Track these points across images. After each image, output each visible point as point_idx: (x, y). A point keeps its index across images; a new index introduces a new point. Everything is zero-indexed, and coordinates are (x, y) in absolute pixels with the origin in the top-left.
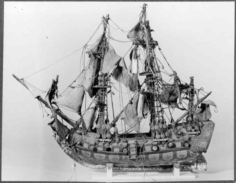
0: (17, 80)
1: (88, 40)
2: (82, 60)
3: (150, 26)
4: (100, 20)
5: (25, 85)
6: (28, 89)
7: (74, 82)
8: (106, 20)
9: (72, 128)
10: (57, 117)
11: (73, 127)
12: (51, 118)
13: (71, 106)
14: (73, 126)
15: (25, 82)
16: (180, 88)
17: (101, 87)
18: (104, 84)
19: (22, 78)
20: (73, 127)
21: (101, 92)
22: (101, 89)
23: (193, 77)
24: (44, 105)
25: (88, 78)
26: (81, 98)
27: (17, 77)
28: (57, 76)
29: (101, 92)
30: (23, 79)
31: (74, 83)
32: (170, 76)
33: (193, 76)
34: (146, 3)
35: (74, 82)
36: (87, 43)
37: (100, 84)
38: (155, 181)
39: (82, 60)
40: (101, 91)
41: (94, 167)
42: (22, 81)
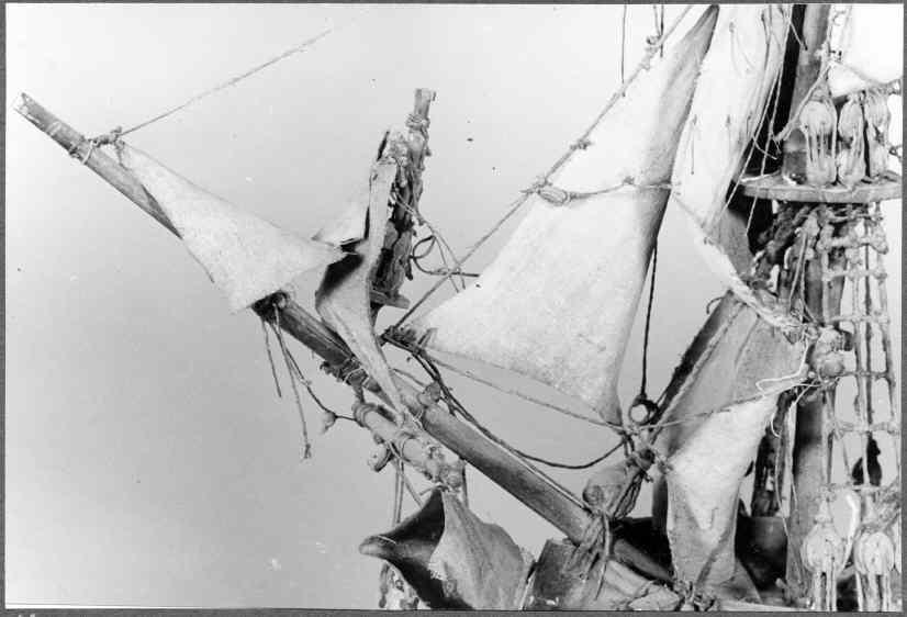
0: (66, 146)
5: (290, 367)
6: (178, 235)
7: (574, 148)
9: (550, 547)
10: (366, 398)
11: (558, 536)
12: (378, 469)
13: (550, 362)
14: (558, 518)
15: (134, 161)
17: (834, 194)
18: (859, 173)
19: (105, 130)
20: (558, 536)
21: (829, 242)
22: (830, 214)
24: (309, 360)
25: (794, 119)
27: (65, 120)
30: (118, 132)
31: (580, 153)
34: (13, 101)
35: (574, 148)
40: (829, 229)
42: (108, 149)
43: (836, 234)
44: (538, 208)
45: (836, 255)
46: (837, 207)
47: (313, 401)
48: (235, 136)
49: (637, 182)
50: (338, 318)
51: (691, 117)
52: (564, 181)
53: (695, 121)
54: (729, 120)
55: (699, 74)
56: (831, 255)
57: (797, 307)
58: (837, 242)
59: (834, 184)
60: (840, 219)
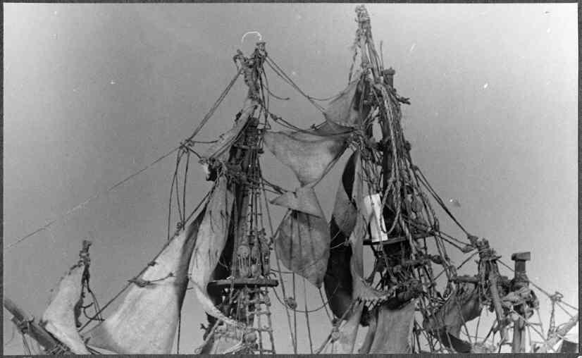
1: (198, 125)
2: (174, 202)
3: (408, 137)
4: (234, 68)
7: (149, 265)
8: (255, 64)
16: (365, 12)
17: (249, 281)
21: (248, 301)
22: (249, 290)
23: (529, 253)
26: (177, 317)
28: (85, 242)
29: (248, 301)
31: (151, 267)
32: (464, 251)
33: (528, 251)
36: (195, 134)
37: (243, 272)
38: (342, 187)
39: (174, 202)
40: (248, 296)
41: (226, 137)
43: (251, 299)
44: (135, 289)
45: (252, 307)
46: (251, 286)
47: (460, 223)
48: (67, 155)
49: (174, 275)
50: (223, 226)
51: (196, 248)
52: (146, 277)
53: (197, 250)
54: (209, 251)
55: (153, 264)
56: (250, 307)
57: (512, 264)
58: (251, 301)
59: (250, 277)
60: (252, 292)
